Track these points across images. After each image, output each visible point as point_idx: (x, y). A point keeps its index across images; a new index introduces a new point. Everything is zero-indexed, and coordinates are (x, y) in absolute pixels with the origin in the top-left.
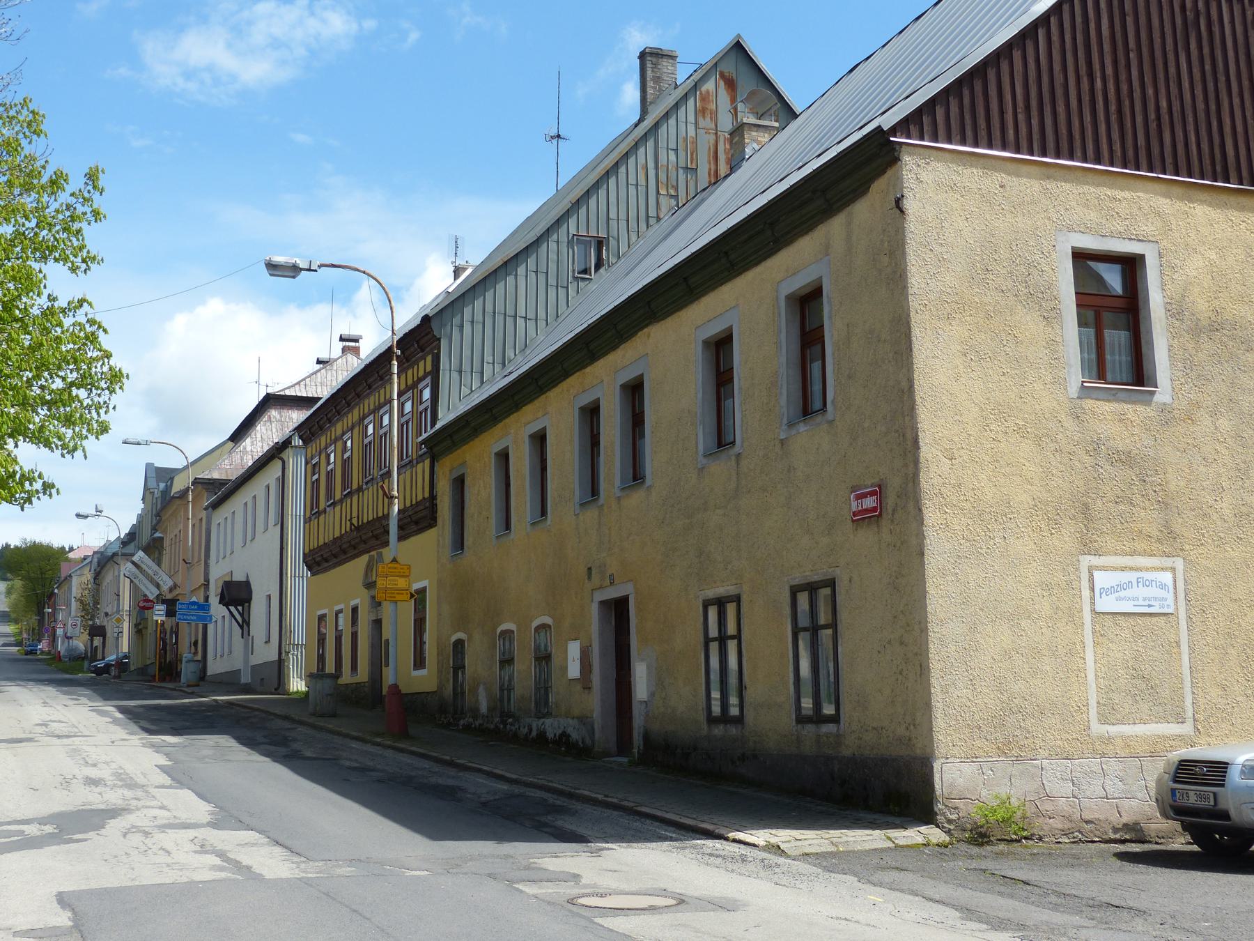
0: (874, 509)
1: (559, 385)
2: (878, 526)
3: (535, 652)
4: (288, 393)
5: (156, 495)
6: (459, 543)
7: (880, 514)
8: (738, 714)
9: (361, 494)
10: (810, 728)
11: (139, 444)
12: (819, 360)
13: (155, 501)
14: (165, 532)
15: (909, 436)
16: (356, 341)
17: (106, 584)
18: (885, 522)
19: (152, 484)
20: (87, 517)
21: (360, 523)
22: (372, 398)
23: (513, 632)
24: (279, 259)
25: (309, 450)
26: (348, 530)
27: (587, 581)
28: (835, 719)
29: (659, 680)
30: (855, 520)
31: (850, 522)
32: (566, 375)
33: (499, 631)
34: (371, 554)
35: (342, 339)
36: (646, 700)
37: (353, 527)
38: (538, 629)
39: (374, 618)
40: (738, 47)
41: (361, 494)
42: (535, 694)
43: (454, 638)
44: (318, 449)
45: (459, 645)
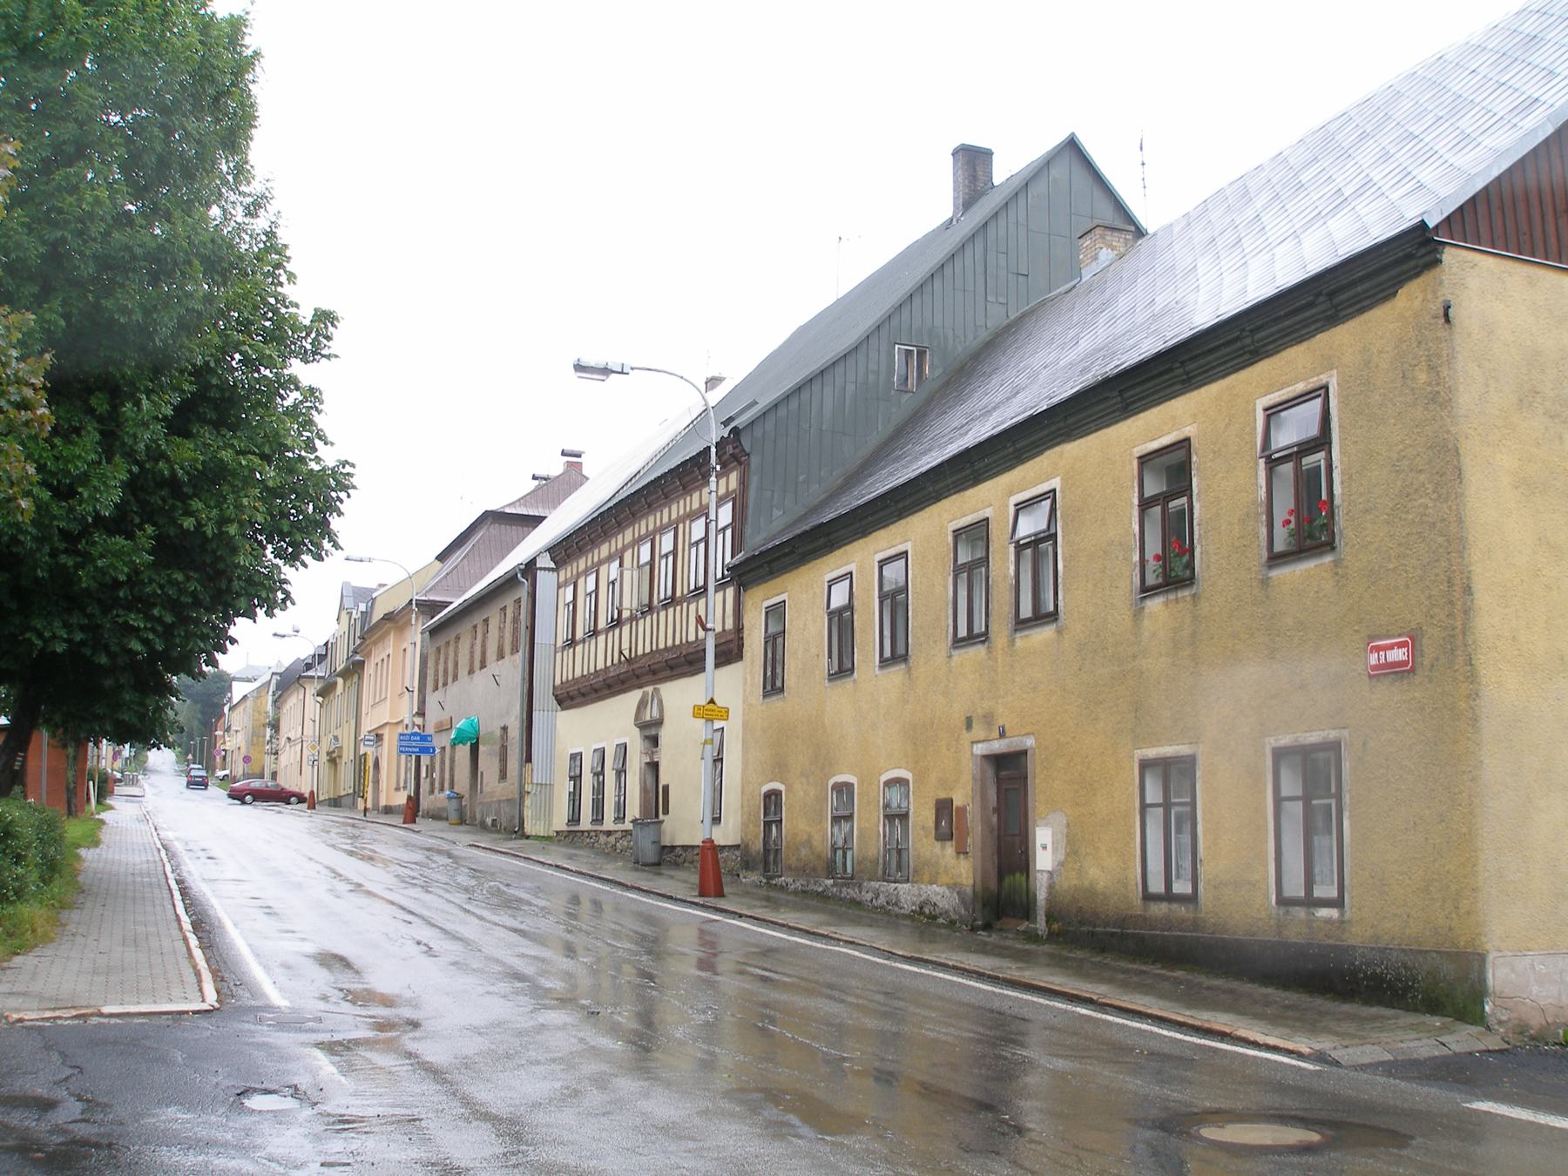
0: (1404, 663)
1: (927, 509)
4: (508, 510)
5: (354, 616)
6: (773, 686)
7: (1412, 670)
8: (1303, 895)
9: (634, 623)
10: (1300, 913)
11: (361, 561)
13: (352, 621)
14: (369, 655)
16: (579, 456)
17: (288, 707)
19: (348, 603)
20: (284, 636)
21: (633, 655)
22: (651, 519)
23: (853, 785)
24: (590, 360)
25: (562, 573)
26: (616, 661)
27: (964, 732)
28: (1338, 903)
29: (1073, 847)
30: (1375, 676)
31: (1366, 678)
32: (937, 497)
33: (831, 783)
34: (646, 689)
35: (564, 453)
37: (623, 658)
38: (889, 783)
39: (648, 760)
40: (1072, 145)
41: (634, 623)
43: (765, 789)
44: (575, 572)
45: (773, 799)
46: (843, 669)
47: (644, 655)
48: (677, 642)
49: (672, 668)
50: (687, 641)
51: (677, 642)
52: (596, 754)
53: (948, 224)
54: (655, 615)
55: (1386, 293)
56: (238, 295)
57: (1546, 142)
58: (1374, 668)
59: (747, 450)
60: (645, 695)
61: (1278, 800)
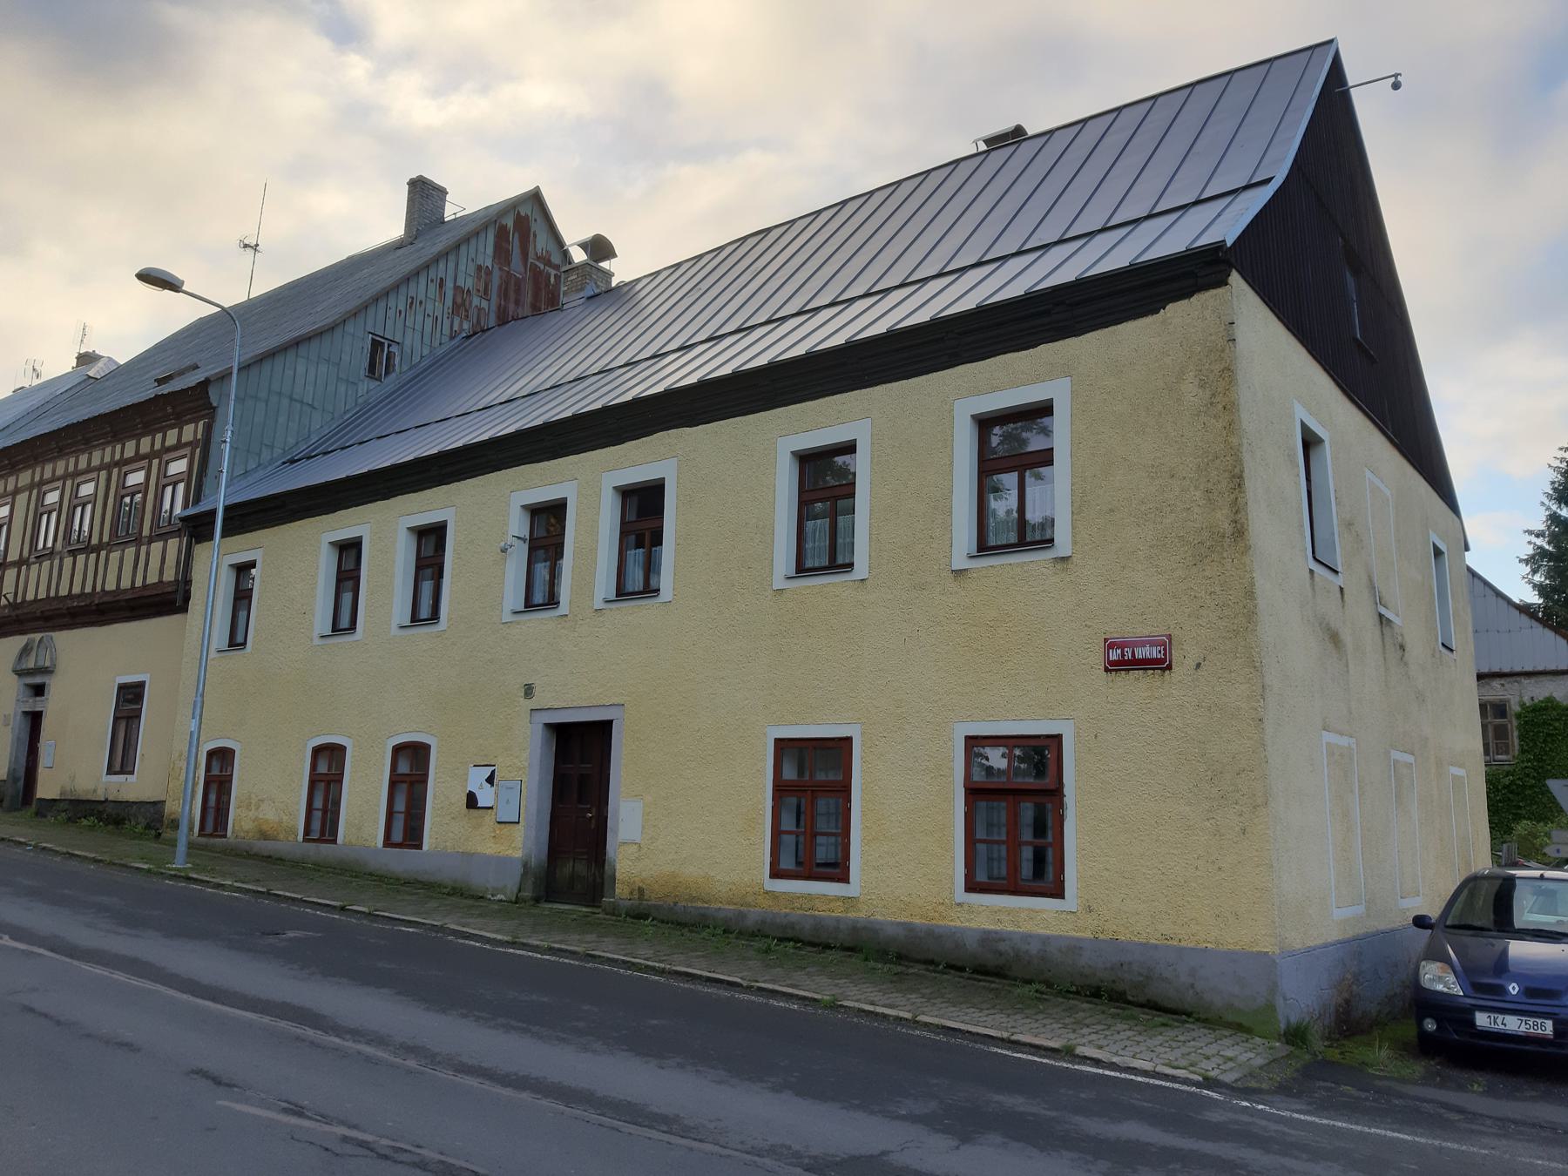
47: (36, 601)
50: (103, 589)
52: (130, 769)
53: (397, 246)
54: (57, 562)
55: (1149, 306)
57: (1273, 196)
59: (215, 404)
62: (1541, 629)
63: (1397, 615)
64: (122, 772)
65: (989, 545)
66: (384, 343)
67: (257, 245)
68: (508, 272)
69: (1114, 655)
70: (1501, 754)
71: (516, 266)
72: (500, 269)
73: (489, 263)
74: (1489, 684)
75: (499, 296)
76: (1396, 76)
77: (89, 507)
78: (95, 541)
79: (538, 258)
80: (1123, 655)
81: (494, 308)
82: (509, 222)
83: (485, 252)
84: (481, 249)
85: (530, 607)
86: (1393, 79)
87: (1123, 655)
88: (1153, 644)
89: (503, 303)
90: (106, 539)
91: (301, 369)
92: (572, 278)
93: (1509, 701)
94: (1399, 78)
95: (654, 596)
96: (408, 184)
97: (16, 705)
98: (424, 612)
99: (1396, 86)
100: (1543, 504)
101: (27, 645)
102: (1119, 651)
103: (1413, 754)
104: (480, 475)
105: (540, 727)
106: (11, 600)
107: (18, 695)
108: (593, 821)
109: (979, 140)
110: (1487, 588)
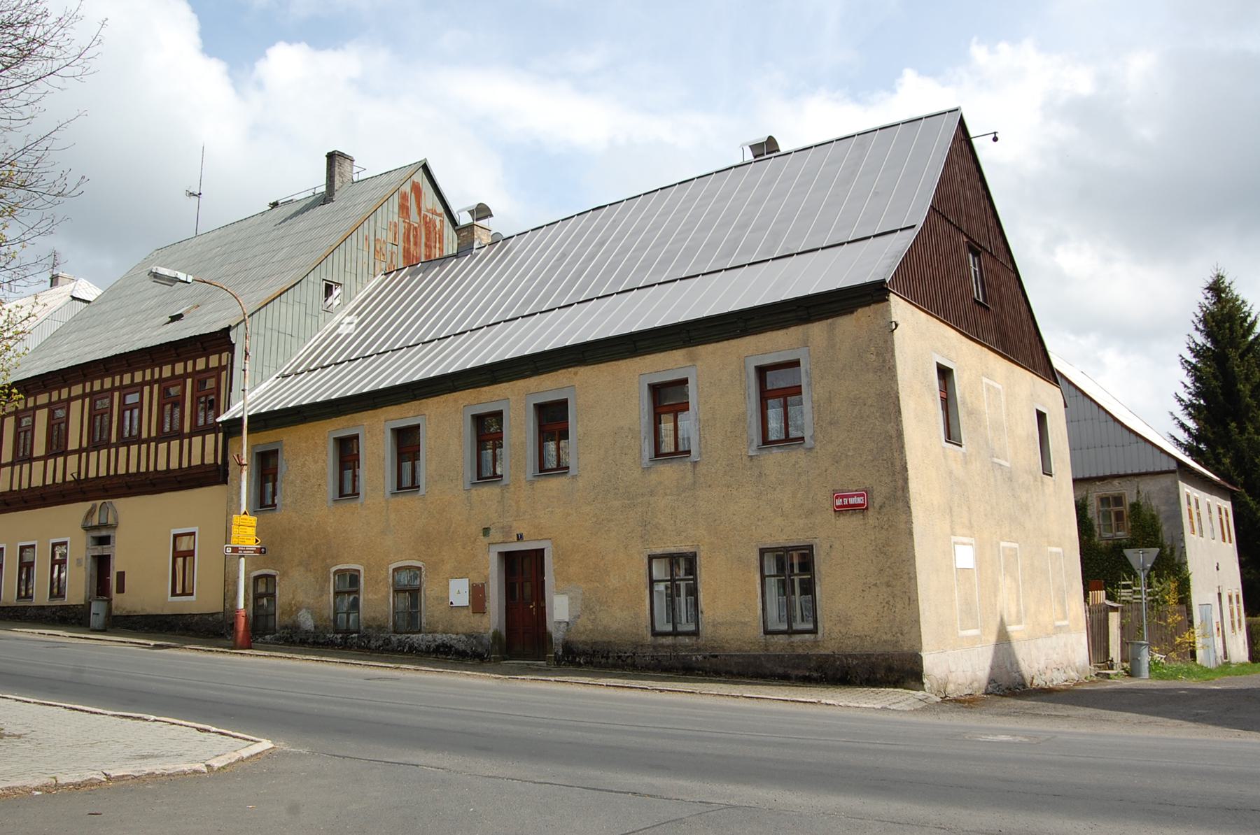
2: (863, 516)
3: (393, 585)
7: (867, 508)
12: (671, 422)
15: (898, 463)
18: (871, 512)
31: (833, 513)
33: (334, 569)
36: (567, 620)
38: (395, 570)
42: (394, 617)
46: (347, 491)
47: (97, 477)
48: (143, 469)
49: (130, 488)
51: (143, 469)
56: (1213, 679)
58: (838, 507)
59: (234, 342)
60: (94, 507)
61: (763, 578)
62: (1143, 443)
63: (1006, 461)
64: (184, 593)
65: (770, 439)
66: (332, 286)
67: (200, 194)
68: (409, 223)
69: (839, 502)
70: (1121, 531)
71: (414, 218)
72: (404, 221)
73: (396, 219)
74: (1111, 483)
75: (404, 242)
76: (995, 133)
77: (136, 412)
78: (144, 435)
79: (428, 211)
80: (843, 502)
81: (401, 250)
82: (407, 188)
83: (391, 211)
84: (391, 209)
85: (483, 479)
86: (993, 135)
87: (843, 502)
88: (858, 496)
89: (406, 246)
90: (153, 434)
91: (283, 310)
92: (464, 234)
93: (1124, 494)
94: (997, 135)
95: (566, 472)
96: (327, 156)
97: (86, 551)
98: (406, 484)
99: (995, 139)
100: (1193, 322)
101: (92, 508)
102: (841, 500)
103: (1017, 543)
104: (442, 394)
105: (496, 553)
106: (76, 478)
107: (87, 544)
108: (534, 609)
109: (745, 145)
110: (1108, 416)
